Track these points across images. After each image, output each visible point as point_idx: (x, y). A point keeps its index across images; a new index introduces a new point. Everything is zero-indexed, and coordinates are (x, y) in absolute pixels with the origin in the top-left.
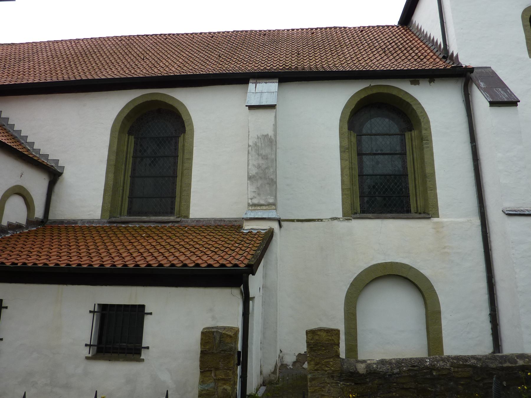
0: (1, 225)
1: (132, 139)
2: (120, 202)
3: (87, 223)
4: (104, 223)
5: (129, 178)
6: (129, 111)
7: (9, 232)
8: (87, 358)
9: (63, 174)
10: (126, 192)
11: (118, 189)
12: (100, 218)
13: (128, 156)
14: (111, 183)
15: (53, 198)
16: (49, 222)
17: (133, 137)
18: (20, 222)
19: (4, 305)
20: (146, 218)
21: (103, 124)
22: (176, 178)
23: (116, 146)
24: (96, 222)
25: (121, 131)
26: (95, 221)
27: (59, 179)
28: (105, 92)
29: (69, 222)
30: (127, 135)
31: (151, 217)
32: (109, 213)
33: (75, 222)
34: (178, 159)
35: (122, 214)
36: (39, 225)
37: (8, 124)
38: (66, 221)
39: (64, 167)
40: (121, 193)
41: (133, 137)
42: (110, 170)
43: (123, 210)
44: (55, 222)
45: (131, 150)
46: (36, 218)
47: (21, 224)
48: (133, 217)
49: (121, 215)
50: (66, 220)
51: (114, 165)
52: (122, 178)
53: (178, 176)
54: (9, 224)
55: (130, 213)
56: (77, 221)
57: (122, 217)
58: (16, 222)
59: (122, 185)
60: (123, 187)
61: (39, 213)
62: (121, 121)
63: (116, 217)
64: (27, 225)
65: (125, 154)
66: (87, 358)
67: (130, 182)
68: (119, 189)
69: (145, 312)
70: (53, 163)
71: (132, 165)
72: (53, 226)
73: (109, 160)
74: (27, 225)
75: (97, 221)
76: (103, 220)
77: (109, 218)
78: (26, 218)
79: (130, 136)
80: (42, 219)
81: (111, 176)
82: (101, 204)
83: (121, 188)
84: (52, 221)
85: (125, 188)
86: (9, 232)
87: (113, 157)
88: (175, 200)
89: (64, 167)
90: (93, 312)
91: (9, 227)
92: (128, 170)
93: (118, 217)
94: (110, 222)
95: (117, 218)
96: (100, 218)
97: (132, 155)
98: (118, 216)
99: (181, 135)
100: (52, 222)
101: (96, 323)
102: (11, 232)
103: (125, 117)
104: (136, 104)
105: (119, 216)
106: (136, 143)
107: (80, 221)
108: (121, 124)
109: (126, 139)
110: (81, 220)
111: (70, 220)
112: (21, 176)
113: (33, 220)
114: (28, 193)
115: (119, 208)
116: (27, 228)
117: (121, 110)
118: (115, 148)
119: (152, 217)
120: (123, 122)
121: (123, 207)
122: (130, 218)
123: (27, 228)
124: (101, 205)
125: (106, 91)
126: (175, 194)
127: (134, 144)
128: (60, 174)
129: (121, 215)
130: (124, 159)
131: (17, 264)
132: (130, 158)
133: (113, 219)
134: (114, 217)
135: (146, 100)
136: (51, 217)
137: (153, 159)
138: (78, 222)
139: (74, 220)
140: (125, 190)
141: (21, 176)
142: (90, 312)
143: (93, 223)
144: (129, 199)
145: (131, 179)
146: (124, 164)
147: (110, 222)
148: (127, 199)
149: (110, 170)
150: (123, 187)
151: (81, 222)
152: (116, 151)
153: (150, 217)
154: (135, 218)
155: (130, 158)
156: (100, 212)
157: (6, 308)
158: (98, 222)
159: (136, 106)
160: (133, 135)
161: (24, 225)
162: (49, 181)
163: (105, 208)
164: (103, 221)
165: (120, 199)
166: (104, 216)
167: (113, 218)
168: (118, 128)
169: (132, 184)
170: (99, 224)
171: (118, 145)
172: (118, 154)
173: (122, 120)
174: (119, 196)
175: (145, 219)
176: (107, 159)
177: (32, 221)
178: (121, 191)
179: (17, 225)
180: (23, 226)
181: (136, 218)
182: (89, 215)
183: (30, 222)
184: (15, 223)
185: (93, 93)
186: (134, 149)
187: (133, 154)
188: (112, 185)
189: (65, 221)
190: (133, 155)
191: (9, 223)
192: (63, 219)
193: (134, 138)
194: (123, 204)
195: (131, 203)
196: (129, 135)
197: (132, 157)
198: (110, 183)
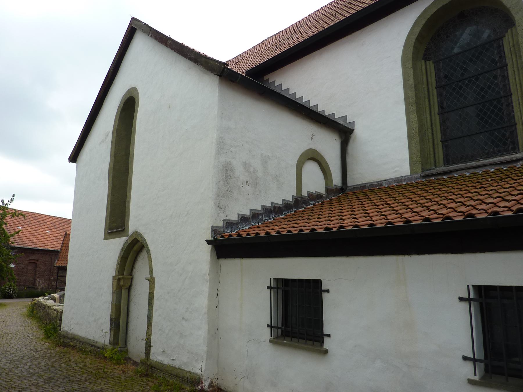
0: (302, 196)
1: (431, 65)
2: (432, 149)
3: (394, 183)
4: (417, 178)
5: (437, 116)
6: (420, 29)
7: (311, 202)
8: (471, 382)
9: (355, 131)
10: (437, 135)
11: (425, 133)
12: (409, 174)
13: (430, 87)
14: (416, 126)
15: (349, 160)
16: (349, 189)
17: (431, 62)
18: (321, 192)
19: (324, 287)
20: (475, 163)
21: (389, 57)
22: (511, 97)
23: (412, 79)
24: (405, 180)
25: (415, 59)
26: (403, 178)
27: (351, 137)
28: (385, 18)
29: (372, 185)
30: (423, 61)
31: (481, 161)
32: (420, 166)
33: (379, 184)
34: (507, 70)
35: (437, 164)
36: (339, 194)
37: (289, 95)
38: (368, 185)
39: (354, 122)
40: (430, 137)
41: (431, 62)
42: (411, 110)
43: (437, 159)
44: (355, 188)
45: (433, 79)
46: (334, 185)
47: (321, 193)
48: (454, 166)
49: (436, 166)
50: (367, 183)
51: (415, 102)
52: (429, 117)
53: (513, 93)
54: (309, 194)
55: (447, 161)
56: (381, 182)
57: (438, 169)
58: (316, 191)
59: (429, 125)
60: (432, 130)
61: (337, 180)
62: (413, 46)
63: (430, 170)
64: (327, 194)
65: (425, 86)
66: (471, 382)
67: (440, 121)
68: (426, 132)
69: (468, 297)
70: (341, 121)
71: (438, 98)
72: (355, 192)
73: (406, 98)
74: (327, 194)
75: (406, 178)
76: (414, 176)
77: (422, 172)
78: (325, 186)
79: (428, 62)
80: (341, 187)
81: (414, 117)
82: (408, 156)
83: (430, 130)
84: (352, 187)
85: (434, 130)
86: (311, 202)
87: (412, 93)
88: (516, 129)
89: (354, 122)
90: (468, 300)
91: (310, 197)
92: (433, 106)
93: (434, 169)
94: (424, 177)
95: (432, 171)
96: (409, 174)
97: (434, 85)
98: (432, 168)
99: (506, 34)
100: (352, 189)
101: (475, 321)
102: (312, 203)
103: (417, 39)
104: (428, 16)
105: (434, 168)
106: (437, 69)
107: (385, 181)
108: (413, 49)
109: (424, 67)
110: (386, 180)
111: (372, 182)
112: (312, 138)
113: (332, 188)
114: (322, 157)
115: (431, 157)
116: (327, 197)
117: (410, 31)
118: (411, 81)
119: (483, 160)
120: (415, 47)
121: (437, 155)
122: (450, 168)
123: (327, 197)
124: (408, 156)
125: (385, 17)
126: (515, 121)
127: (435, 71)
128: (351, 131)
129: (436, 166)
130: (426, 92)
131: (331, 229)
132: (432, 89)
133: (428, 172)
134: (427, 170)
135: (441, 5)
136: (350, 182)
137: (467, 82)
138: (382, 183)
139: (377, 182)
140: (435, 133)
141: (312, 138)
142: (461, 299)
143: (401, 182)
144: (442, 143)
145: (440, 117)
146: (427, 99)
147: (424, 177)
148: (440, 143)
149: (411, 110)
150: (432, 130)
151: (386, 182)
152: (413, 84)
153: (479, 161)
154: (457, 166)
155: (432, 89)
156: (409, 166)
157: (328, 291)
158: (408, 178)
159: (429, 19)
160: (431, 60)
161: (324, 194)
162: (340, 142)
163: (414, 160)
164: (414, 177)
165: (431, 145)
166: (415, 170)
167: (426, 171)
168: (410, 55)
169: (443, 122)
170: (410, 180)
171: (414, 76)
172: (416, 87)
173: (413, 44)
174: (429, 141)
175: (474, 164)
176: (404, 98)
177: (331, 189)
178: (430, 134)
179: (317, 195)
180: (323, 195)
181: (458, 166)
182: (394, 172)
183: (330, 191)
184: (315, 192)
185: (370, 26)
186: (436, 77)
187: (436, 83)
188: (418, 127)
189: (367, 185)
190: (436, 86)
191: (309, 193)
192: (364, 182)
193: (434, 63)
194: (436, 151)
195: (446, 148)
196: (425, 62)
197: (436, 88)
198: (414, 126)
